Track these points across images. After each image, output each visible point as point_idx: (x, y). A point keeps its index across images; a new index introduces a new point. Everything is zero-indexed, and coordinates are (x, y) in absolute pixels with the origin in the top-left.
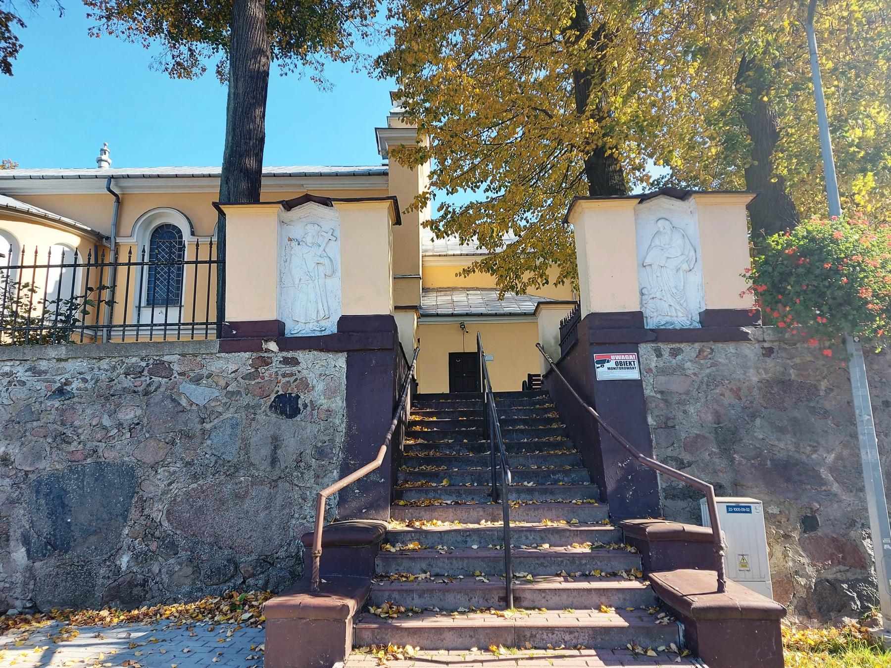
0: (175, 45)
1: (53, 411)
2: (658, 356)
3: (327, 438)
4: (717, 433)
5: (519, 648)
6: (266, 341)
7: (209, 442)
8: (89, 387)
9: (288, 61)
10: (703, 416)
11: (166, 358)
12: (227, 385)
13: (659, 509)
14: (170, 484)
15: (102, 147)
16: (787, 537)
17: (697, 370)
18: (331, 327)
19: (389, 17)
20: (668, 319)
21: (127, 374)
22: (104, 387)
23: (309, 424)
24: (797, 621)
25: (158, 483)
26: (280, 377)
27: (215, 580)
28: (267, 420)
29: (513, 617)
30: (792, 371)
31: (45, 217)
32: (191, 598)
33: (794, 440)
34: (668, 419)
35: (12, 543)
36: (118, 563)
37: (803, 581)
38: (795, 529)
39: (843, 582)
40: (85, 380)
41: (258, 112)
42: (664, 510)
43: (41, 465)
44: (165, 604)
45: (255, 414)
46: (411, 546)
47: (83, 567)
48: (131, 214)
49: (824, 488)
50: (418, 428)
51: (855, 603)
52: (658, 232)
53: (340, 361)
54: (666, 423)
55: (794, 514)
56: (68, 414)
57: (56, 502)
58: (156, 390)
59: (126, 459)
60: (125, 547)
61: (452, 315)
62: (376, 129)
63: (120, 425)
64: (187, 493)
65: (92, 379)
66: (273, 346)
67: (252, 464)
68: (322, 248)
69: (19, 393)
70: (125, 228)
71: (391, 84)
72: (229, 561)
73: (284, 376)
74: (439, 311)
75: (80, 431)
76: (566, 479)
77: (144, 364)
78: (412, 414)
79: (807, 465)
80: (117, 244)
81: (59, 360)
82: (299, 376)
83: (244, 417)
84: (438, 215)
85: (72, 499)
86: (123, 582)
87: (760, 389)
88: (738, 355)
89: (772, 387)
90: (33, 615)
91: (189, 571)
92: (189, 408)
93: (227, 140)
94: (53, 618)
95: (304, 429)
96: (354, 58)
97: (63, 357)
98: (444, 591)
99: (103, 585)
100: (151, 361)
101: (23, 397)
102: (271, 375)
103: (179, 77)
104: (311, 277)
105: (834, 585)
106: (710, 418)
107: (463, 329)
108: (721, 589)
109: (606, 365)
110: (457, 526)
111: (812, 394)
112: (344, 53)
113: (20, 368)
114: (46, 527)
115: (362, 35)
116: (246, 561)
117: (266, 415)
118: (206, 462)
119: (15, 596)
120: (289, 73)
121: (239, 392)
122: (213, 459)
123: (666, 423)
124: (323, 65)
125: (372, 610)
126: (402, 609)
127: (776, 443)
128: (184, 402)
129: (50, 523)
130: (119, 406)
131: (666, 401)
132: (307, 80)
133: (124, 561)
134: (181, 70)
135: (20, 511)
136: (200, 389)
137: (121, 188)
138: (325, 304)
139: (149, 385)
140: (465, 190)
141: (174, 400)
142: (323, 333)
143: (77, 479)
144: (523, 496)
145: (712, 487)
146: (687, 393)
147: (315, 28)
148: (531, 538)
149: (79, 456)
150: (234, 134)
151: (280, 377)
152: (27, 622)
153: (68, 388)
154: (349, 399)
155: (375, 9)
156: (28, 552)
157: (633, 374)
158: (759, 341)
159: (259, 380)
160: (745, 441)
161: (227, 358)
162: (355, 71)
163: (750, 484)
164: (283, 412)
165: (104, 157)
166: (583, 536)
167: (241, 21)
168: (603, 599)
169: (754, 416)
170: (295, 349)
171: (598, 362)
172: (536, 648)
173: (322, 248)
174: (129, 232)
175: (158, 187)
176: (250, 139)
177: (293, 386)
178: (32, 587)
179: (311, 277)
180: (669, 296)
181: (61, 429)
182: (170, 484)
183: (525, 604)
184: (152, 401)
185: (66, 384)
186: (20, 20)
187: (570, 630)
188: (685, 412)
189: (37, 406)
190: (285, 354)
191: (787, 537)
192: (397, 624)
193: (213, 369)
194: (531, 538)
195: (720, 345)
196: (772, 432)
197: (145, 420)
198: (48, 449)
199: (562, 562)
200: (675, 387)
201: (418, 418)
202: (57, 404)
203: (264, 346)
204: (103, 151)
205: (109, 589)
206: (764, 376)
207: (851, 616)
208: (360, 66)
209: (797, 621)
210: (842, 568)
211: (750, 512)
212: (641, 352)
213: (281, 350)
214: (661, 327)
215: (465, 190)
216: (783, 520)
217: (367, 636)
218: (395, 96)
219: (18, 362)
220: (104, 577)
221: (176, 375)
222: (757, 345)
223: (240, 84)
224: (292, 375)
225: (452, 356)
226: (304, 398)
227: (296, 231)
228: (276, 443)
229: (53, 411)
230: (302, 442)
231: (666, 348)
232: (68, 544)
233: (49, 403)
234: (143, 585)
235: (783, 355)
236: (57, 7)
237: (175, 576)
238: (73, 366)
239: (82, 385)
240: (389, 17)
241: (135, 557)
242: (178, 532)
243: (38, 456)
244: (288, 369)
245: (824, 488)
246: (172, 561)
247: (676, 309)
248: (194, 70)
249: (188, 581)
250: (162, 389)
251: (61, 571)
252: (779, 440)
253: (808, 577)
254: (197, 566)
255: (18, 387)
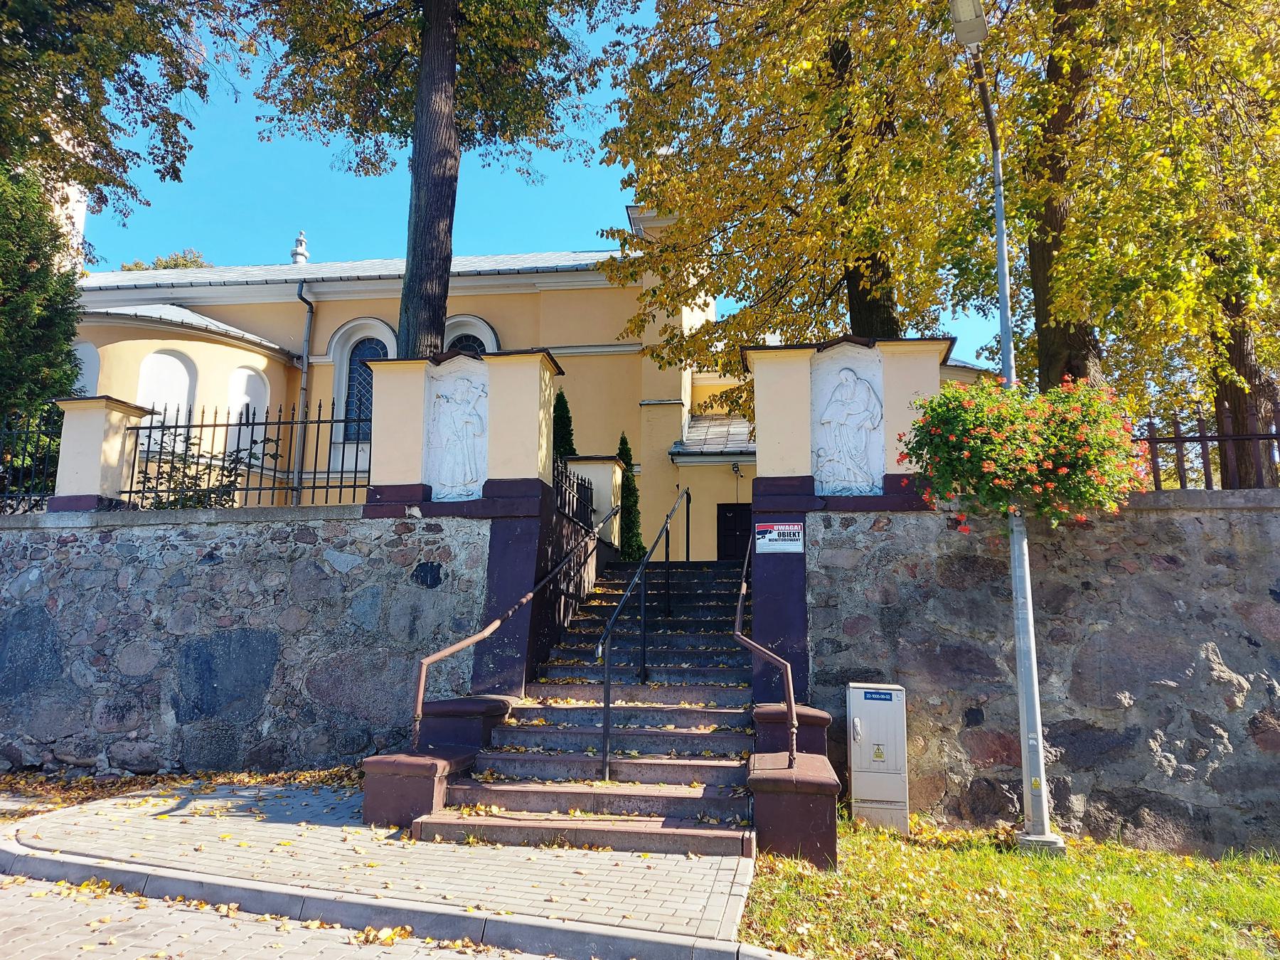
0: (359, 138)
1: (204, 576)
2: (826, 527)
3: (465, 610)
4: (882, 614)
5: (596, 813)
6: (410, 506)
7: (350, 611)
8: (237, 552)
9: (492, 148)
10: (869, 594)
11: (311, 524)
12: (371, 552)
13: (806, 695)
14: (310, 653)
15: (298, 236)
16: (945, 730)
17: (869, 543)
18: (477, 492)
19: (615, 86)
20: (845, 484)
21: (273, 540)
22: (251, 553)
23: (449, 595)
24: (945, 821)
25: (299, 651)
26: (423, 545)
27: (349, 750)
28: (408, 590)
29: (601, 787)
30: (978, 546)
31: (226, 335)
32: (326, 766)
33: (969, 624)
34: (830, 597)
35: (163, 706)
36: (260, 728)
37: (957, 779)
38: (956, 722)
39: (1004, 783)
40: (233, 545)
41: (443, 225)
42: (812, 695)
43: (192, 629)
44: (301, 770)
45: (396, 583)
46: (535, 722)
47: (227, 731)
48: (326, 327)
49: (997, 679)
50: (595, 603)
51: (1014, 806)
52: (841, 384)
53: (484, 529)
54: (827, 602)
55: (958, 705)
56: (217, 579)
57: (204, 667)
58: (300, 556)
59: (270, 626)
60: (267, 713)
61: (721, 454)
62: (627, 207)
63: (265, 592)
64: (327, 663)
65: (240, 544)
66: (416, 511)
67: (390, 635)
68: (471, 405)
69: (172, 557)
70: (320, 345)
71: (619, 171)
72: (363, 731)
73: (427, 543)
74: (706, 449)
75: (228, 597)
76: (730, 661)
77: (289, 529)
78: (596, 585)
79: (981, 652)
80: (310, 365)
81: (209, 524)
82: (442, 544)
83: (385, 586)
84: (660, 340)
85: (219, 664)
86: (264, 747)
87: (939, 566)
88: (918, 527)
89: (952, 564)
90: (180, 775)
91: (325, 739)
92: (331, 575)
93: (408, 261)
94: (197, 778)
95: (444, 599)
96: (566, 145)
97: (213, 521)
98: (544, 762)
99: (245, 749)
100: (296, 527)
101: (175, 561)
102: (414, 542)
103: (366, 174)
104: (458, 437)
105: (992, 785)
106: (877, 597)
107: (736, 472)
108: (790, 766)
109: (768, 536)
110: (581, 704)
111: (999, 573)
112: (553, 139)
113: (172, 532)
114: (194, 692)
115: (574, 117)
116: (380, 732)
117: (407, 584)
118: (346, 631)
119: (165, 756)
120: (494, 163)
121: (381, 560)
122: (353, 629)
123: (827, 602)
124: (530, 153)
125: (474, 776)
126: (503, 777)
127: (949, 627)
128: (327, 569)
129: (198, 687)
130: (265, 572)
131: (830, 577)
132: (512, 173)
133: (265, 727)
134: (368, 165)
135: (170, 675)
136: (344, 556)
137: (315, 294)
138: (473, 466)
139: (294, 551)
140: (692, 309)
141: (317, 567)
142: (470, 498)
143: (224, 644)
144: (673, 677)
145: (789, 665)
146: (855, 568)
147: (516, 113)
148: (658, 718)
149: (226, 622)
150: (415, 255)
151: (423, 545)
152: (174, 780)
153: (218, 553)
154: (490, 571)
155: (596, 78)
156: (177, 714)
157: (796, 547)
158: (945, 511)
159: (402, 547)
160: (914, 624)
161: (369, 524)
162: (568, 160)
163: (911, 672)
164: (424, 582)
165: (300, 250)
166: (704, 716)
167: (424, 118)
168: (697, 776)
169: (926, 597)
170: (439, 515)
171: (759, 533)
172: (612, 814)
173: (471, 405)
174: (324, 350)
175: (359, 292)
176: (433, 259)
177: (436, 554)
178: (180, 749)
179: (458, 437)
180: (848, 458)
181: (210, 594)
182: (310, 653)
183: (621, 777)
184: (296, 567)
185: (215, 549)
186: (188, 122)
187: (646, 799)
188: (850, 590)
189: (188, 570)
190: (428, 520)
191: (945, 730)
192: (487, 786)
193: (357, 535)
194: (658, 718)
195: (900, 515)
196: (945, 615)
197: (289, 587)
198: (198, 614)
199: (674, 741)
200: (840, 562)
201: (599, 591)
202: (207, 569)
203: (407, 512)
204: (299, 242)
205: (251, 754)
206: (945, 551)
207: (1006, 820)
208: (574, 152)
209: (945, 821)
210: (1005, 767)
211: (891, 700)
212: (808, 522)
213: (424, 516)
214: (837, 494)
215: (692, 309)
216: (945, 712)
217: (459, 795)
218: (627, 183)
219: (171, 526)
220: (246, 742)
221: (320, 541)
222: (942, 516)
223: (422, 194)
224: (435, 543)
225: (722, 509)
226: (446, 567)
227: (444, 387)
228: (415, 614)
229: (204, 576)
230: (441, 613)
231: (836, 518)
232: (214, 708)
233: (199, 568)
234: (282, 751)
235: (971, 527)
236: (231, 92)
237: (312, 744)
238: (222, 530)
239: (230, 550)
240: (615, 86)
241: (276, 723)
242: (317, 701)
243: (189, 622)
244: (431, 536)
245: (997, 679)
246: (309, 729)
247: (855, 474)
248: (383, 165)
249: (324, 749)
250: (306, 556)
251: (206, 734)
252: (952, 624)
253: (964, 775)
254: (333, 735)
255: (171, 551)
